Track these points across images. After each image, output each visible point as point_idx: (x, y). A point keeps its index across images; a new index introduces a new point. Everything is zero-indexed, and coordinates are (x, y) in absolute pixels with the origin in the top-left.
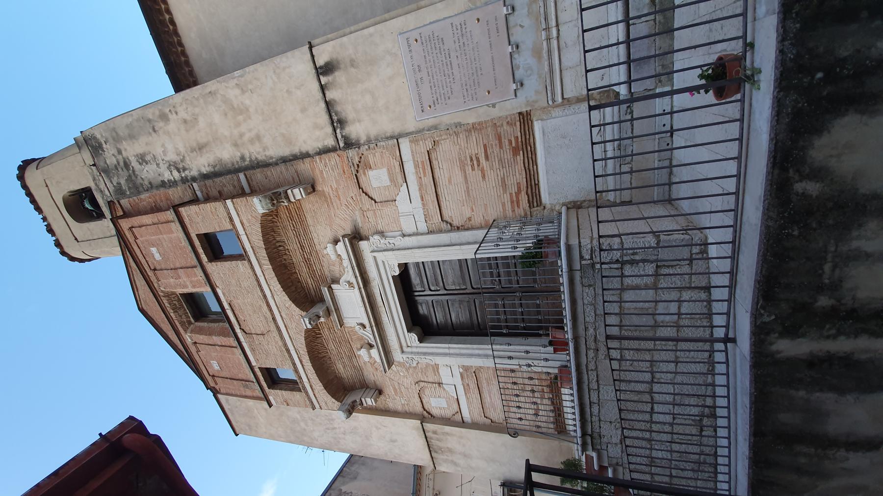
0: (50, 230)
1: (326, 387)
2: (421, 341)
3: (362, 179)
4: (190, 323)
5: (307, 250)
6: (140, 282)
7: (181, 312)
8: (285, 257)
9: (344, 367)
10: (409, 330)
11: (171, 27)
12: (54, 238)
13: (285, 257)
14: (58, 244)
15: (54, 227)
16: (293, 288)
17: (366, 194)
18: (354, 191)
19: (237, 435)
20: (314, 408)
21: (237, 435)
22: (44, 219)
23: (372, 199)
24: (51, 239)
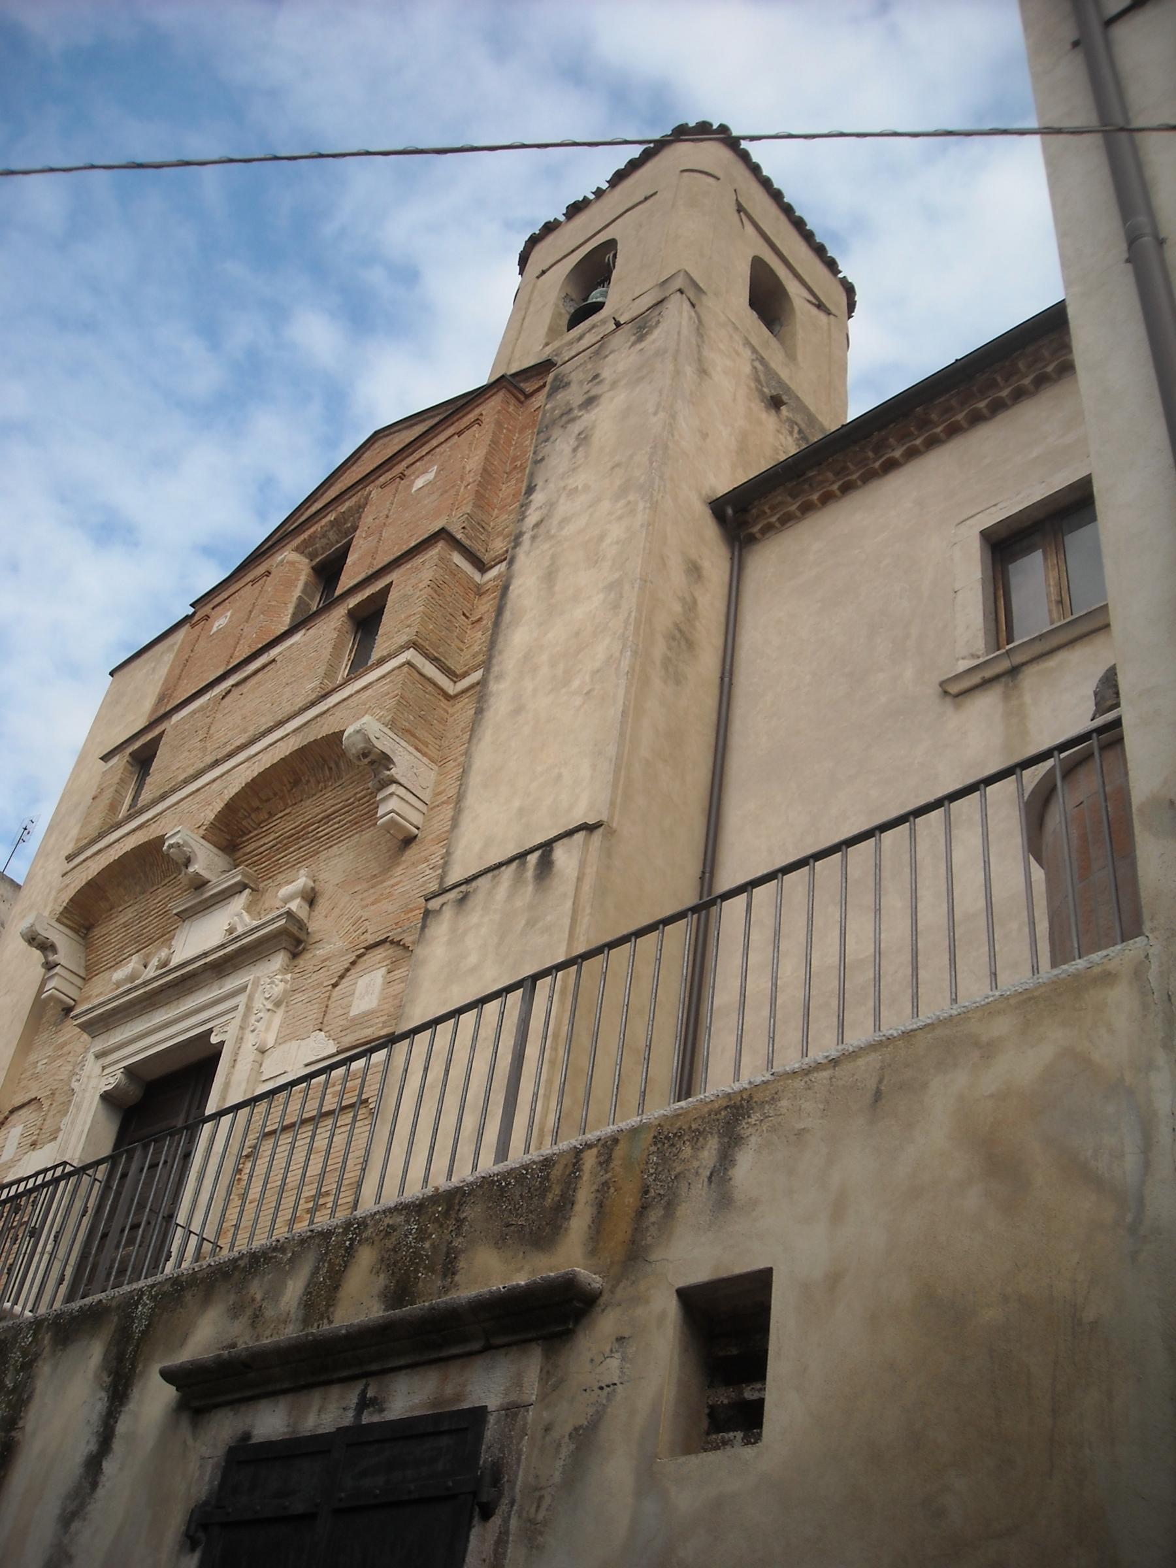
0: (575, 209)
1: (90, 884)
2: (106, 1097)
3: (380, 954)
4: (311, 557)
5: (324, 830)
6: (465, 401)
7: (332, 535)
8: (313, 780)
9: (125, 925)
10: (129, 1071)
11: (877, 465)
12: (562, 218)
13: (313, 780)
14: (550, 228)
15: (581, 219)
16: (256, 803)
17: (353, 963)
18: (371, 939)
19: (112, 674)
20: (69, 858)
21: (112, 674)
22: (599, 193)
23: (342, 977)
24: (557, 212)
